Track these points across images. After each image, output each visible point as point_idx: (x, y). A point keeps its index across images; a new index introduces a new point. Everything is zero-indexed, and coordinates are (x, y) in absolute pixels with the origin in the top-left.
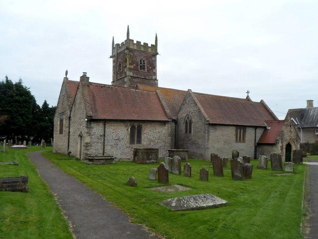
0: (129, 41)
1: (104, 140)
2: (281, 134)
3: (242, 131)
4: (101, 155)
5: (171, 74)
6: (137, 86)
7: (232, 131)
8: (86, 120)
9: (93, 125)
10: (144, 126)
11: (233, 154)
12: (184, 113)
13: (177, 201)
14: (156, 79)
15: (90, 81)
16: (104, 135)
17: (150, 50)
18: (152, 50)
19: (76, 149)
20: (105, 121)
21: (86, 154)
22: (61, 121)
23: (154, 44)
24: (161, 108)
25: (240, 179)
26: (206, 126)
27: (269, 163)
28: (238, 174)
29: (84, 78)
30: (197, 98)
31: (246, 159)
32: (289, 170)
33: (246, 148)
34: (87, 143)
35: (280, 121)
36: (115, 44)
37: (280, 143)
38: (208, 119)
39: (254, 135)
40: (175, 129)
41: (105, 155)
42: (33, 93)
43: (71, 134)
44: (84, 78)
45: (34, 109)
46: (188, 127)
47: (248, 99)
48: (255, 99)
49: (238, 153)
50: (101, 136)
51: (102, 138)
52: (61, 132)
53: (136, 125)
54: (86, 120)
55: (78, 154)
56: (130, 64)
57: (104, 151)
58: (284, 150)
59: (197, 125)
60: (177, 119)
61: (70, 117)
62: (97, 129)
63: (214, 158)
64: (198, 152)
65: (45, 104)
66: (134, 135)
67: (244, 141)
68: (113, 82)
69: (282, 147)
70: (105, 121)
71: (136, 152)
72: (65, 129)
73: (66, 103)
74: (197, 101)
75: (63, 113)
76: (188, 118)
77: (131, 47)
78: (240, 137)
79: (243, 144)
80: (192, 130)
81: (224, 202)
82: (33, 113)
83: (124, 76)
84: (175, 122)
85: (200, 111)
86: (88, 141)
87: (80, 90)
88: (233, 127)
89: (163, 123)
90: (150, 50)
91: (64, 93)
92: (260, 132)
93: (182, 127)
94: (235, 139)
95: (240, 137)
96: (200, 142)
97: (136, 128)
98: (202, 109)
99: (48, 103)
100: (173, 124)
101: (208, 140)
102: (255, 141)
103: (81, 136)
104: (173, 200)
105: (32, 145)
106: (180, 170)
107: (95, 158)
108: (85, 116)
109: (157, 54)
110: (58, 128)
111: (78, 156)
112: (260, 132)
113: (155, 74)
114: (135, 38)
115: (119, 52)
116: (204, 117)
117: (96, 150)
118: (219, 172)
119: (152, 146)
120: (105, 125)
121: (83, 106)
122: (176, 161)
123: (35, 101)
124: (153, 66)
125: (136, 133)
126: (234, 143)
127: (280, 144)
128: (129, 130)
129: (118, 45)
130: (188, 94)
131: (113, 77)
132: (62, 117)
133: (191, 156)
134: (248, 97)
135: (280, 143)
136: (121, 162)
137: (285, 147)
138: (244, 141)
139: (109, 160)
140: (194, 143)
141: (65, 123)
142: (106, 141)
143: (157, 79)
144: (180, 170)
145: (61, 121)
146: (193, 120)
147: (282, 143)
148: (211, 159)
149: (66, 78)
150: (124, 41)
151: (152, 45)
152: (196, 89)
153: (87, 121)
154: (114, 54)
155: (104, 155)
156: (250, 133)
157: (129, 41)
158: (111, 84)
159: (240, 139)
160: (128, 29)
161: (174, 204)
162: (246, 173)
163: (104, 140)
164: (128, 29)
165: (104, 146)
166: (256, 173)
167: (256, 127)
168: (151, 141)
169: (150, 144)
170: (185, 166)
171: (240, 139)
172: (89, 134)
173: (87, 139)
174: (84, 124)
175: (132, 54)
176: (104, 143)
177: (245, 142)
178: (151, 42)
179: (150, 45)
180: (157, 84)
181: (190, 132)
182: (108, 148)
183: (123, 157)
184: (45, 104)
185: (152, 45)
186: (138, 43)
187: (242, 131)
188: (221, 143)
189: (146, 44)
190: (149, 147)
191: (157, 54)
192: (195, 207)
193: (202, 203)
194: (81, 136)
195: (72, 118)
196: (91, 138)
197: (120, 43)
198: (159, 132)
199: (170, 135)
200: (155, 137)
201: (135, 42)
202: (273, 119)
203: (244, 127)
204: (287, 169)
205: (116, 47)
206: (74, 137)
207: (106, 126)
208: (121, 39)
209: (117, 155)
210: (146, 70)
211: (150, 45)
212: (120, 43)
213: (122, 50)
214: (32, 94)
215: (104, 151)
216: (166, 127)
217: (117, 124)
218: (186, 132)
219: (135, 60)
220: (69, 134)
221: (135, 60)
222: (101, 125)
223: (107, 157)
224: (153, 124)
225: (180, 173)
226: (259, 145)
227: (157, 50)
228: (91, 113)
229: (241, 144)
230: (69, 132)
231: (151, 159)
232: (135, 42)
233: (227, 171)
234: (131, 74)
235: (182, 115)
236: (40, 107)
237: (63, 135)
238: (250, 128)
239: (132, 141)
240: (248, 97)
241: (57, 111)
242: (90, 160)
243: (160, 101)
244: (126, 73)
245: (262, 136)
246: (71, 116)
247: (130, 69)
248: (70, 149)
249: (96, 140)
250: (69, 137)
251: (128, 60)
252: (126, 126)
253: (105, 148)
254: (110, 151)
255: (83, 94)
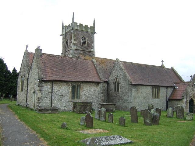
0: (74, 23)
1: (52, 97)
2: (186, 93)
3: (157, 89)
4: (49, 107)
5: (104, 49)
6: (79, 56)
7: (149, 89)
8: (38, 80)
9: (44, 84)
10: (82, 85)
11: (149, 107)
12: (114, 76)
13: (91, 140)
14: (93, 52)
15: (42, 52)
16: (52, 92)
17: (89, 30)
18: (91, 30)
19: (32, 103)
20: (53, 82)
21: (38, 106)
22: (23, 82)
23: (92, 26)
24: (95, 73)
25: (150, 125)
26: (130, 86)
27: (175, 114)
28: (148, 121)
29: (38, 50)
30: (123, 65)
31: (159, 111)
32: (190, 119)
33: (160, 102)
34: (39, 98)
35: (185, 83)
36: (64, 26)
37: (185, 98)
38: (131, 81)
39: (166, 93)
40: (107, 88)
41: (52, 107)
42: (6, 62)
43: (28, 91)
44: (38, 50)
45: (6, 74)
46: (117, 86)
47: (163, 66)
48: (168, 66)
49: (153, 106)
50: (49, 93)
51: (51, 94)
52: (22, 90)
53: (76, 84)
54: (38, 80)
55: (33, 106)
56: (75, 40)
57: (51, 104)
58: (188, 104)
59: (123, 85)
60: (109, 81)
61: (28, 79)
62: (47, 88)
63: (133, 110)
64: (124, 105)
65: (14, 70)
66: (75, 92)
67: (158, 97)
68: (62, 53)
69: (186, 102)
70: (53, 82)
71: (75, 105)
72: (25, 88)
73: (26, 68)
74: (123, 67)
75: (24, 76)
76: (117, 80)
77: (76, 28)
78: (155, 95)
79: (158, 99)
80: (119, 89)
81: (129, 141)
82: (5, 76)
83: (70, 49)
84: (107, 83)
85: (125, 75)
86: (40, 96)
87: (35, 58)
88: (150, 87)
89: (97, 83)
90: (89, 30)
91: (25, 61)
92: (170, 90)
93: (112, 87)
94: (151, 96)
95: (155, 95)
96: (125, 98)
97: (76, 87)
98: (126, 73)
99: (16, 69)
100: (105, 85)
101: (131, 96)
102: (167, 97)
103: (35, 93)
104: (88, 139)
105: (14, 100)
106: (105, 118)
107: (43, 109)
108: (38, 78)
109: (95, 33)
110: (20, 87)
111: (33, 108)
112: (170, 90)
113: (93, 48)
114: (78, 21)
115: (66, 31)
116: (128, 79)
117: (46, 103)
118: (135, 120)
119: (88, 100)
120: (52, 84)
121: (36, 70)
122: (103, 111)
123: (7, 68)
124: (92, 40)
125: (75, 92)
126: (151, 99)
127: (185, 100)
128: (71, 88)
129: (66, 26)
130: (115, 62)
131: (63, 50)
132: (23, 78)
133: (119, 109)
134: (162, 65)
135: (185, 98)
136: (65, 112)
137: (188, 101)
138: (158, 97)
139: (54, 110)
140: (121, 99)
141: (25, 83)
142: (53, 97)
143: (95, 51)
144: (105, 118)
145: (23, 82)
146: (120, 82)
147: (186, 98)
148: (131, 109)
149: (26, 51)
150: (70, 23)
151: (91, 27)
152: (121, 60)
153: (39, 82)
154: (63, 34)
155: (51, 107)
156: (163, 91)
157: (74, 23)
158: (61, 55)
159: (156, 95)
160: (73, 15)
161: (88, 143)
162: (155, 121)
163: (52, 97)
164: (73, 15)
165: (52, 100)
166: (162, 120)
167: (167, 87)
168: (87, 97)
169: (87, 99)
170: (109, 115)
171: (156, 95)
172: (40, 91)
173: (39, 95)
174: (37, 84)
175: (76, 33)
176: (52, 98)
177: (159, 98)
178: (90, 25)
179: (89, 27)
180: (94, 55)
181: (118, 91)
182: (55, 102)
183: (66, 108)
184: (14, 70)
185: (91, 27)
186: (81, 25)
187: (157, 89)
188: (140, 99)
189: (86, 26)
190: (86, 101)
191: (95, 33)
192: (105, 144)
193: (112, 142)
194: (35, 93)
195: (29, 80)
196: (42, 94)
197: (68, 25)
198: (94, 91)
199: (102, 93)
200: (90, 94)
201: (78, 24)
202: (180, 81)
203: (158, 87)
204: (188, 118)
205: (64, 28)
206: (30, 93)
207: (53, 86)
208: (68, 22)
209: (61, 107)
210: (86, 45)
211: (89, 27)
212: (68, 25)
213: (69, 30)
214: (5, 62)
215: (51, 104)
216: (99, 87)
217: (61, 84)
218: (115, 91)
219: (79, 37)
220: (27, 91)
221: (79, 37)
222: (50, 84)
223: (53, 108)
224: (89, 84)
225: (105, 121)
226: (170, 100)
227: (95, 30)
228: (42, 76)
229: (156, 99)
230: (27, 90)
231: (86, 111)
232: (78, 24)
233: (141, 120)
234: (75, 47)
235: (112, 78)
236: (10, 72)
237: (23, 92)
238: (163, 88)
239: (73, 97)
240: (162, 65)
241: (20, 74)
242: (40, 110)
243: (95, 68)
244: (71, 47)
245: (172, 94)
246: (29, 78)
247: (74, 44)
248: (28, 102)
249: (45, 96)
250: (27, 93)
251: (73, 37)
252: (68, 86)
253: (53, 102)
254: (56, 104)
255: (37, 62)
